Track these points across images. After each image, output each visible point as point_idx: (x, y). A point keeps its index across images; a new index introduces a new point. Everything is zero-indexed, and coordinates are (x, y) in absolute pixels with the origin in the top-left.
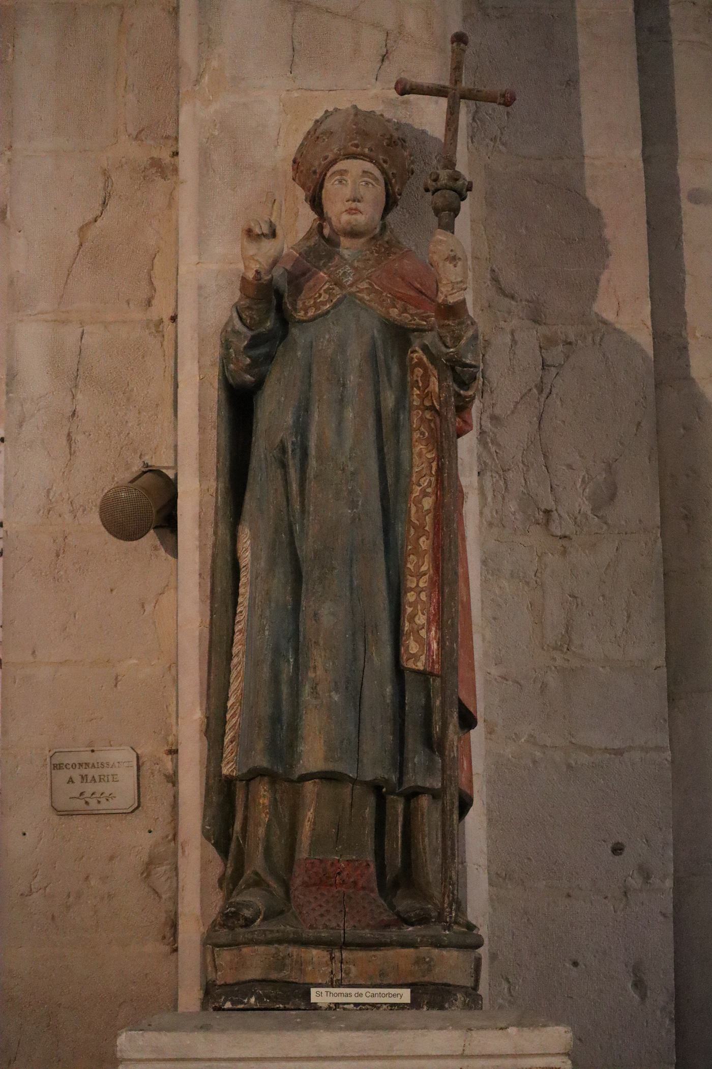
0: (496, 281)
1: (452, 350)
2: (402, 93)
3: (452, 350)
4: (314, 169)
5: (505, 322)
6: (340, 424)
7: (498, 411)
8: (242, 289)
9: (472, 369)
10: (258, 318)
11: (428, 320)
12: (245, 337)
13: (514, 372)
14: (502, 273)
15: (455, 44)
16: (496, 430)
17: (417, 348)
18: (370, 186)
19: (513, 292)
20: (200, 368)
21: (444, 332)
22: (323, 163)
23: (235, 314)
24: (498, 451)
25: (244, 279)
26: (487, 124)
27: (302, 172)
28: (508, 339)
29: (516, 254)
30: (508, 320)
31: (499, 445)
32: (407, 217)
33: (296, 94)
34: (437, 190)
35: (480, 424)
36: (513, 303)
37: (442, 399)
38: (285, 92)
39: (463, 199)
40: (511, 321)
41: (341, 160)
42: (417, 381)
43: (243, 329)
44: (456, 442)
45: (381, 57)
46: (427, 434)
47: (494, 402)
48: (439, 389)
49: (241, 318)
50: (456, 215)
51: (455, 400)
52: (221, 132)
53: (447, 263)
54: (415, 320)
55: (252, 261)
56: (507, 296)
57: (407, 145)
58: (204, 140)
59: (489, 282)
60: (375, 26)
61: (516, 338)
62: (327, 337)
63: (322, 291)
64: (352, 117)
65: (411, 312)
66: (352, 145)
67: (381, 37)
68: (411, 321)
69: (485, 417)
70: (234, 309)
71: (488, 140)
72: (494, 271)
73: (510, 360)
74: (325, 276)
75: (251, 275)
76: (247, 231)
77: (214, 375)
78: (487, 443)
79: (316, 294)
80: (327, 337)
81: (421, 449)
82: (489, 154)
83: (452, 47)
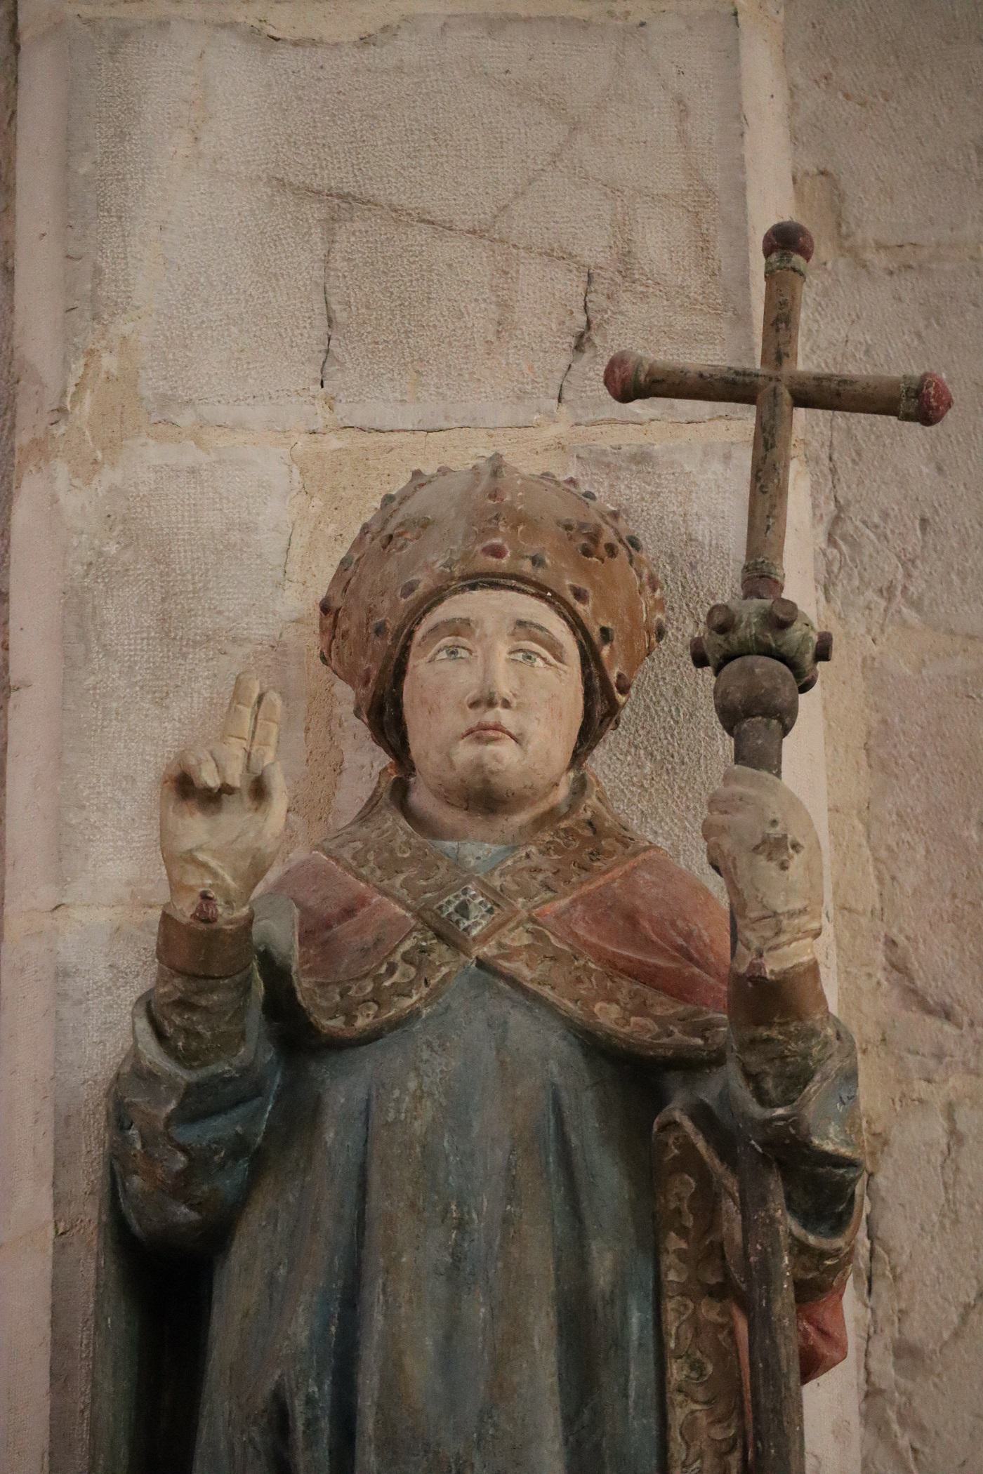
0: (899, 970)
1: (780, 1111)
2: (625, 395)
3: (780, 1111)
4: (378, 620)
5: (929, 1081)
6: (448, 1338)
7: (916, 1332)
8: (165, 949)
9: (841, 1171)
10: (209, 1034)
11: (707, 1034)
12: (173, 1088)
13: (956, 1222)
14: (916, 949)
15: (774, 257)
16: (910, 1386)
17: (678, 1116)
18: (539, 662)
19: (948, 1000)
20: (56, 1203)
21: (752, 1059)
22: (403, 600)
23: (143, 1024)
24: (918, 1445)
25: (166, 919)
26: (868, 550)
27: (345, 635)
28: (938, 1129)
29: (954, 896)
30: (937, 1078)
31: (920, 1428)
32: (647, 770)
33: (334, 442)
34: (728, 658)
35: (866, 1368)
36: (948, 1028)
37: (752, 1259)
38: (305, 437)
39: (804, 688)
40: (946, 1081)
41: (455, 592)
42: (678, 1211)
43: (165, 1064)
44: (799, 1395)
45: (573, 341)
46: (710, 1368)
47: (903, 1305)
48: (745, 1231)
49: (160, 1035)
50: (786, 731)
51: (793, 1266)
52: (126, 546)
53: (762, 861)
54: (670, 1034)
55: (190, 867)
56: (930, 1011)
57: (643, 556)
58: (79, 567)
59: (880, 975)
60: (557, 255)
61: (961, 1126)
62: (412, 1085)
63: (397, 957)
64: (485, 480)
65: (659, 1011)
66: (484, 550)
67: (569, 285)
68: (658, 1036)
69: (878, 1347)
70: (141, 1011)
71: (870, 594)
72: (894, 943)
73: (946, 1188)
74: (409, 915)
75: (185, 909)
76: (176, 781)
77: (90, 1213)
78: (887, 1423)
79: (381, 965)
80: (412, 1085)
81: (693, 1412)
82: (875, 630)
83: (768, 264)
